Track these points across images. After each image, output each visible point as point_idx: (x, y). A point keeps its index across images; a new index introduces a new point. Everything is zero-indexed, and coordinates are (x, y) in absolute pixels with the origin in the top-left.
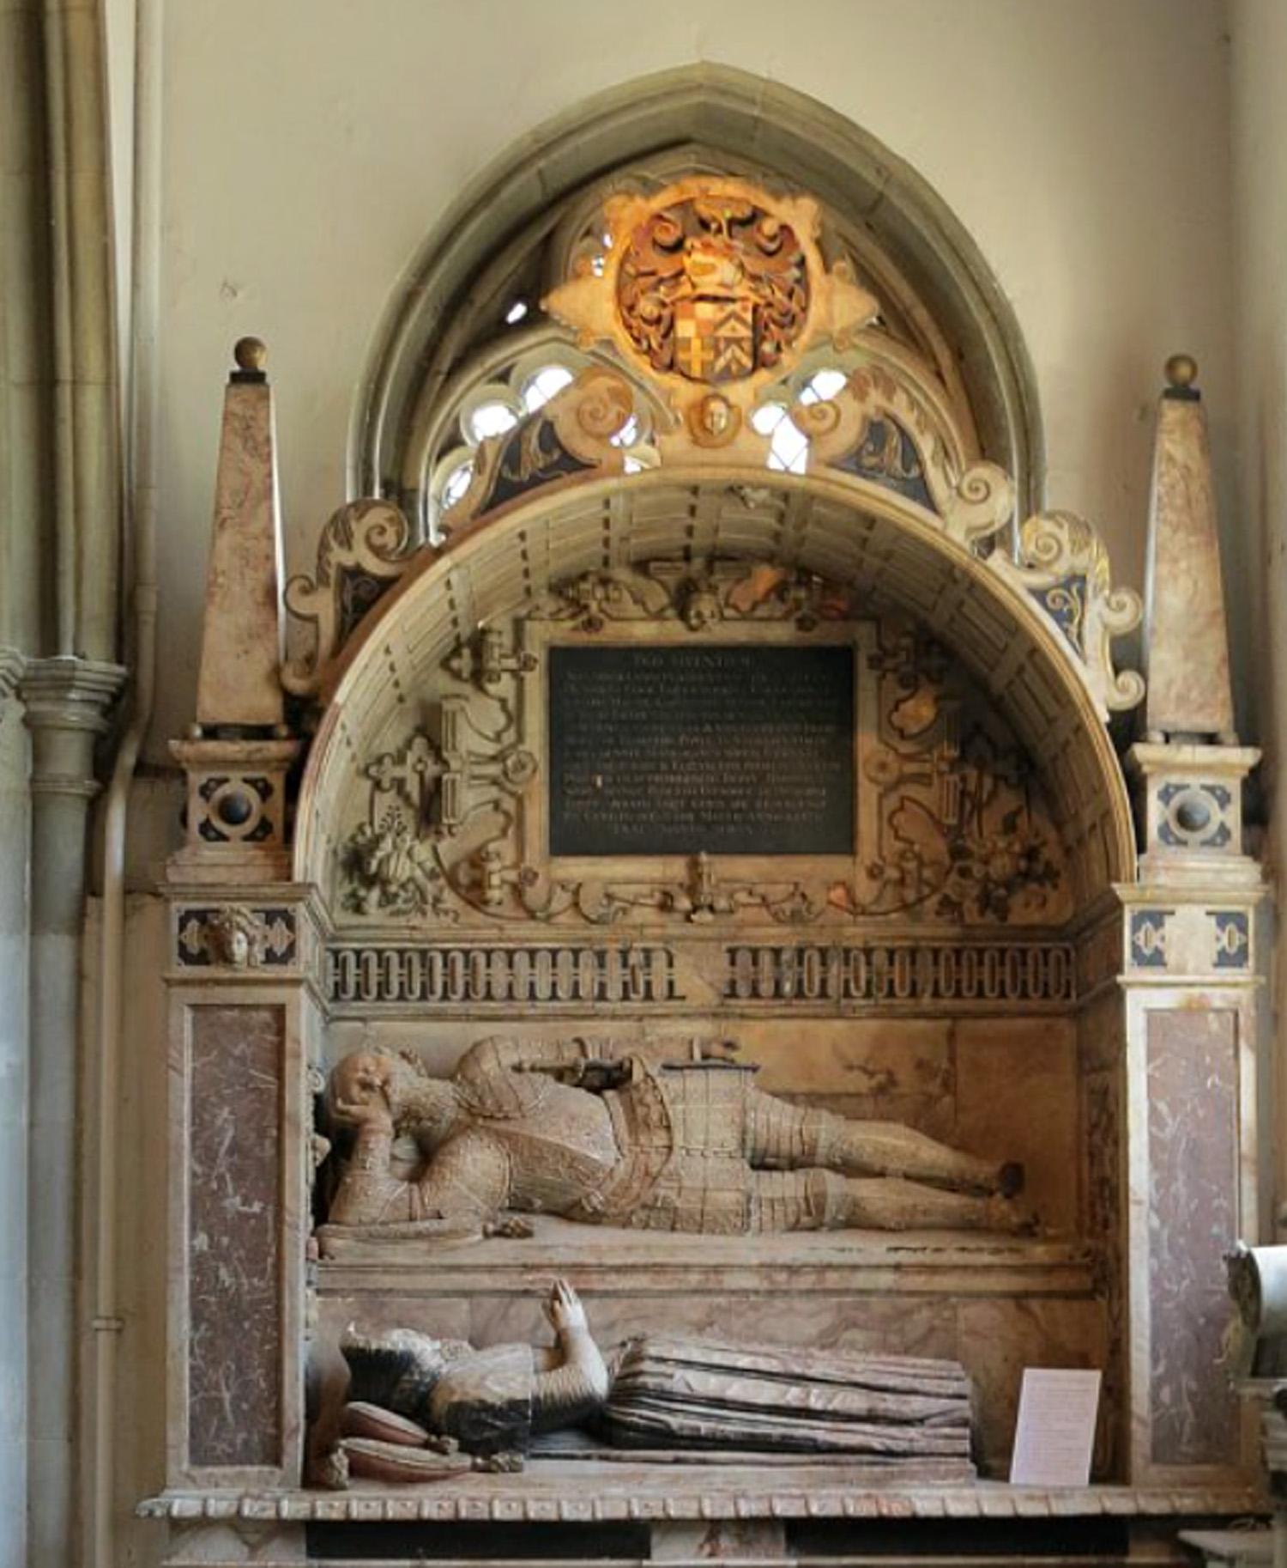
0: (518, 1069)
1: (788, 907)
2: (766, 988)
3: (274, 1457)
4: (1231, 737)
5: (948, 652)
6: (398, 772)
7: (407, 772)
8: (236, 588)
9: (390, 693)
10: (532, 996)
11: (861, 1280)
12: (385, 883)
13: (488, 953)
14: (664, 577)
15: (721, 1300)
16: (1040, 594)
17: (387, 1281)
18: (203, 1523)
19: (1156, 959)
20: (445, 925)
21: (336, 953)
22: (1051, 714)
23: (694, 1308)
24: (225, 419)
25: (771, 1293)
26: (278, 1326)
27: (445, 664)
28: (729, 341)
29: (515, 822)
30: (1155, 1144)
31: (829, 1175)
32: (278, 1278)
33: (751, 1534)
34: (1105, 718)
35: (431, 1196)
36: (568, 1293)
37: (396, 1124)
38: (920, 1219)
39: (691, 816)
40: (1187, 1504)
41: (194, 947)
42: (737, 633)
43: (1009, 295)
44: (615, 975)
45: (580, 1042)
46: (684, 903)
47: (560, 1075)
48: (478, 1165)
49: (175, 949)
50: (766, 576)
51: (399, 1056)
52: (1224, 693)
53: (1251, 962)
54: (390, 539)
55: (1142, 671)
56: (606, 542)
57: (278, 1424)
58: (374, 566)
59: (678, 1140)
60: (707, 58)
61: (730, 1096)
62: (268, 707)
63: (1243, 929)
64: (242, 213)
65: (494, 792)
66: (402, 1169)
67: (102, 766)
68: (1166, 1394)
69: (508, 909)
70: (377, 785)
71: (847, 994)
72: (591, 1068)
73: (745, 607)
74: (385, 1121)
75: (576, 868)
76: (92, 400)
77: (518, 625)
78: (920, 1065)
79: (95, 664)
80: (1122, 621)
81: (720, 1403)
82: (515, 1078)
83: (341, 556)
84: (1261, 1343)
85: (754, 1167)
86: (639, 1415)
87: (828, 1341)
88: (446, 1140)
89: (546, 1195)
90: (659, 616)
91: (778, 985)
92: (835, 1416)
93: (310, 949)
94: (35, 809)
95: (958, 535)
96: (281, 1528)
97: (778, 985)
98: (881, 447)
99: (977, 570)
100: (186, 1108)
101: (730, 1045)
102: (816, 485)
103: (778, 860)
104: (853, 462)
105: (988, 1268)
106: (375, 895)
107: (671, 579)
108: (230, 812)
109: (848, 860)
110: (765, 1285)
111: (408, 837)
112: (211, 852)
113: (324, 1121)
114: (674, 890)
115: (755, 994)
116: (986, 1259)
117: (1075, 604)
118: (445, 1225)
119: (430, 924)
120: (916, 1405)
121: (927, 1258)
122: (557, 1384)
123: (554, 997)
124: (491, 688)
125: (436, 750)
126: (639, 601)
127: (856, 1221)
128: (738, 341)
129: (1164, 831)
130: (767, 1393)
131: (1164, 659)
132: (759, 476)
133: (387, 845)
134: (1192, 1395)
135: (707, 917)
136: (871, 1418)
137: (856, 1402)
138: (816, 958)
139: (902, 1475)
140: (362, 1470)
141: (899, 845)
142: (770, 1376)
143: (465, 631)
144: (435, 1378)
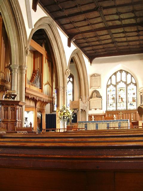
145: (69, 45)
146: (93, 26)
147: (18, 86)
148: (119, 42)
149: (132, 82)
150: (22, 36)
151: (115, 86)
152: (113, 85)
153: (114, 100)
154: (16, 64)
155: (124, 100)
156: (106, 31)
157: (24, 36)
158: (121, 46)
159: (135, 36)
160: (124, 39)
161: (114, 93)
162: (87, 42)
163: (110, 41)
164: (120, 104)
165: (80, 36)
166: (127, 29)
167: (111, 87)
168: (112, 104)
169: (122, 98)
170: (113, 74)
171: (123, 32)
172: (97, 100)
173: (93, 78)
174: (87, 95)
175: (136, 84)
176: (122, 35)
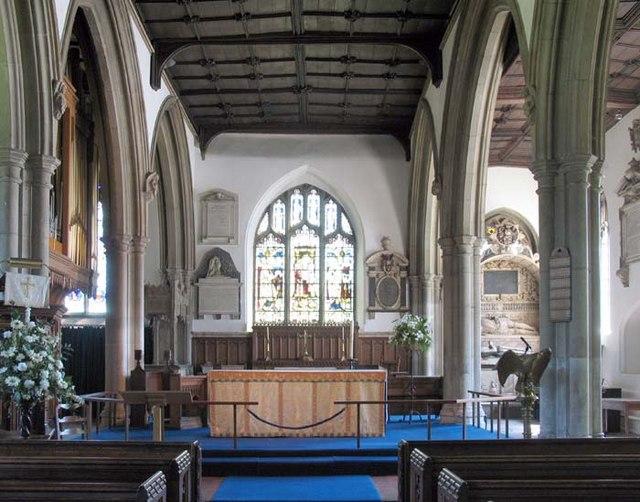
75: (487, 295)
98: (525, 252)
145: (155, 83)
146: (251, 23)
147: (24, 238)
148: (317, 90)
149: (339, 230)
150: (41, 36)
151: (284, 239)
152: (276, 235)
153: (279, 287)
154: (18, 147)
155: (314, 290)
156: (287, 47)
157: (48, 34)
158: (317, 104)
159: (376, 76)
160: (339, 83)
161: (280, 262)
162: (209, 77)
163: (289, 82)
164: (296, 303)
165: (191, 52)
166: (361, 50)
167: (271, 242)
168: (271, 300)
169: (305, 282)
170: (280, 197)
171: (344, 59)
172: (224, 284)
173: (211, 204)
174: (190, 266)
175: (352, 239)
176: (335, 67)
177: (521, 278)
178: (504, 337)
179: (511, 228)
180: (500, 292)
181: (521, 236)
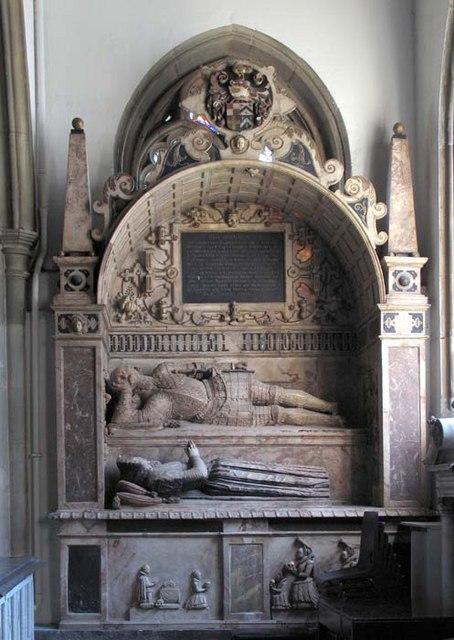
0: (174, 372)
1: (263, 320)
2: (256, 347)
3: (95, 499)
4: (417, 254)
5: (316, 233)
6: (131, 275)
7: (134, 275)
8: (75, 205)
9: (128, 246)
10: (178, 350)
11: (290, 441)
12: (127, 312)
13: (163, 336)
14: (221, 209)
15: (244, 448)
16: (352, 205)
17: (131, 442)
18: (71, 520)
19: (392, 330)
20: (148, 326)
21: (111, 336)
22: (353, 250)
23: (234, 450)
24: (70, 146)
25: (261, 445)
26: (96, 454)
27: (146, 239)
28: (245, 117)
29: (171, 291)
30: (392, 393)
31: (280, 408)
32: (95, 439)
33: (257, 524)
34: (375, 248)
35: (145, 414)
36: (193, 445)
37: (133, 391)
38: (309, 421)
39: (229, 290)
40: (403, 513)
41: (64, 326)
42: (245, 227)
43: (339, 106)
44: (205, 343)
45: (195, 364)
46: (228, 319)
47: (188, 374)
48: (161, 405)
49: (57, 328)
50: (254, 208)
51: (134, 367)
52: (415, 239)
53: (424, 331)
54: (128, 187)
55: (386, 230)
56: (201, 193)
57: (96, 487)
58: (123, 196)
59: (229, 394)
60: (234, 22)
61: (245, 380)
62: (87, 245)
63: (421, 320)
64: (74, 91)
65: (164, 281)
66: (136, 406)
67: (31, 270)
68: (395, 477)
69: (169, 321)
70: (124, 279)
71: (283, 349)
72: (199, 372)
73: (247, 218)
74: (129, 389)
75: (191, 307)
76: (23, 139)
77: (171, 225)
78: (307, 372)
79: (27, 231)
80: (381, 214)
81: (246, 480)
82: (172, 375)
83: (111, 193)
84: (440, 452)
85: (254, 405)
86: (219, 484)
87: (279, 461)
88: (150, 396)
89: (186, 414)
90: (218, 222)
91: (259, 346)
92: (284, 484)
93: (103, 332)
94: (7, 281)
95: (324, 183)
96: (98, 522)
97: (259, 346)
98: (297, 154)
99: (331, 196)
100: (62, 381)
101: (244, 364)
102: (276, 167)
103: (260, 304)
104: (288, 159)
105: (333, 437)
106: (124, 316)
107: (222, 210)
108: (74, 281)
109: (282, 304)
110: (258, 443)
111: (135, 296)
112: (69, 295)
113: (109, 390)
114: (224, 314)
115: (252, 349)
116: (332, 434)
117: (364, 208)
118: (151, 423)
119: (143, 326)
120: (311, 481)
121: (313, 433)
122: (191, 473)
123: (185, 350)
124: (162, 246)
125: (144, 267)
126: (211, 217)
127: (288, 422)
128: (248, 117)
129: (395, 286)
130: (261, 477)
131: (393, 226)
132: (256, 163)
133: (128, 299)
134: (404, 477)
135: (236, 323)
136: (296, 485)
137: (291, 480)
138: (272, 337)
139: (307, 504)
140: (125, 503)
141: (299, 299)
142: (262, 471)
143: (153, 226)
144: (149, 471)
177: (296, 256)
178: (240, 431)
179: (251, 77)
180: (231, 295)
181: (284, 104)
